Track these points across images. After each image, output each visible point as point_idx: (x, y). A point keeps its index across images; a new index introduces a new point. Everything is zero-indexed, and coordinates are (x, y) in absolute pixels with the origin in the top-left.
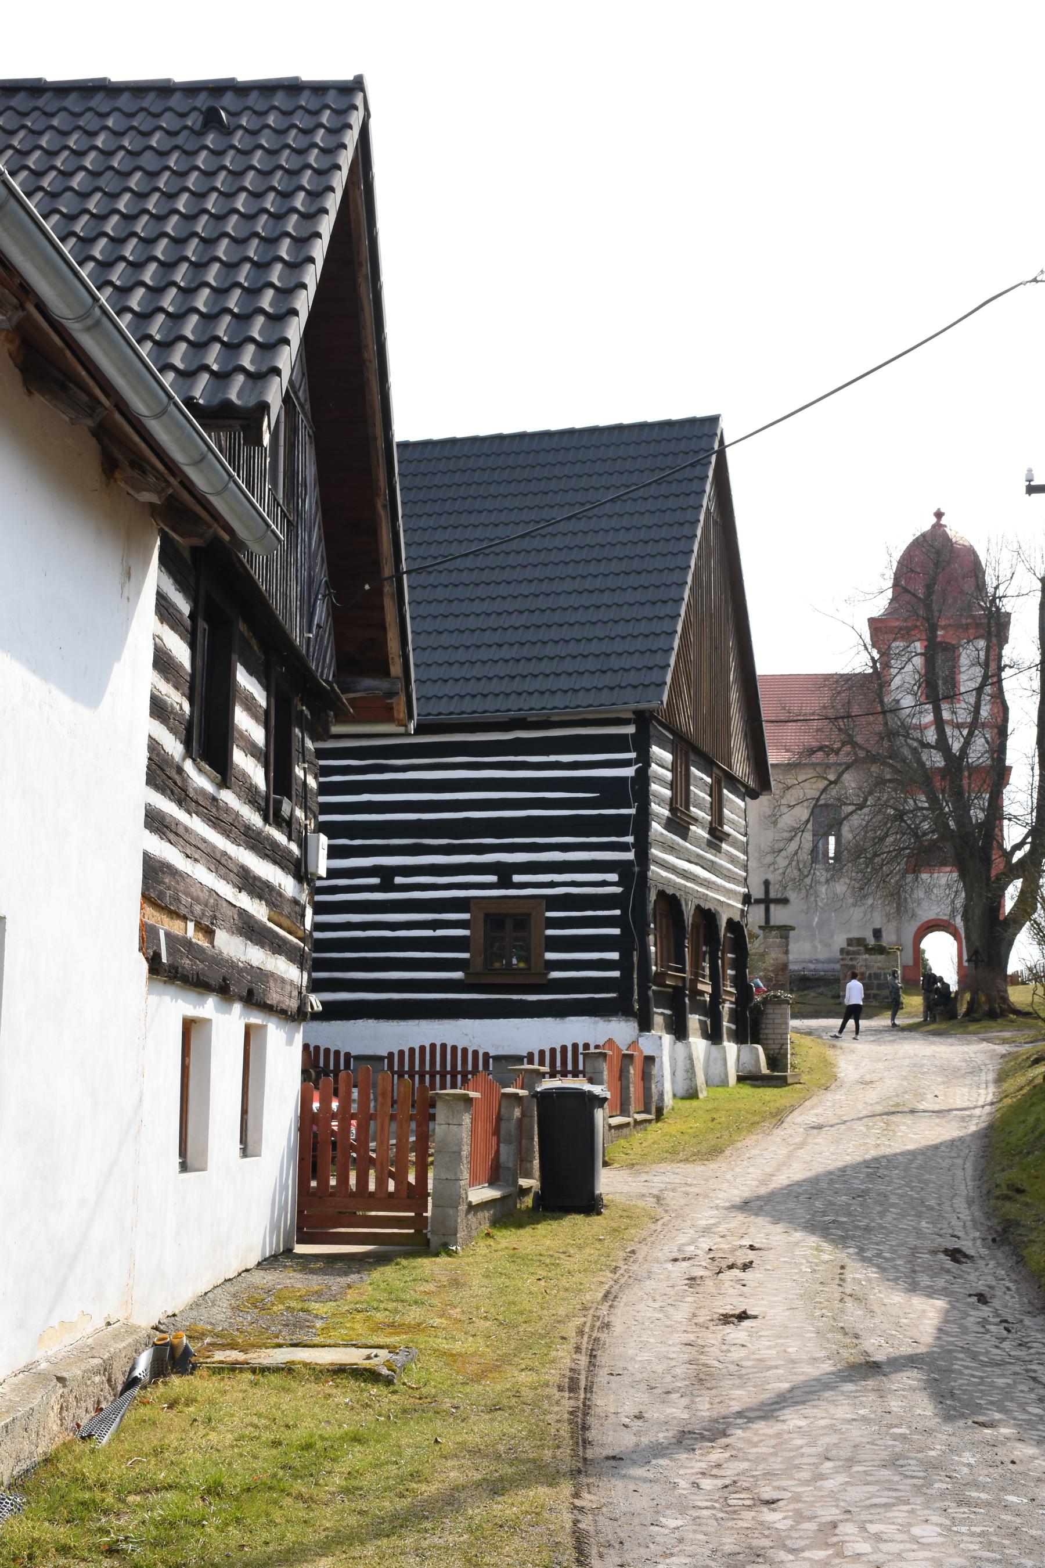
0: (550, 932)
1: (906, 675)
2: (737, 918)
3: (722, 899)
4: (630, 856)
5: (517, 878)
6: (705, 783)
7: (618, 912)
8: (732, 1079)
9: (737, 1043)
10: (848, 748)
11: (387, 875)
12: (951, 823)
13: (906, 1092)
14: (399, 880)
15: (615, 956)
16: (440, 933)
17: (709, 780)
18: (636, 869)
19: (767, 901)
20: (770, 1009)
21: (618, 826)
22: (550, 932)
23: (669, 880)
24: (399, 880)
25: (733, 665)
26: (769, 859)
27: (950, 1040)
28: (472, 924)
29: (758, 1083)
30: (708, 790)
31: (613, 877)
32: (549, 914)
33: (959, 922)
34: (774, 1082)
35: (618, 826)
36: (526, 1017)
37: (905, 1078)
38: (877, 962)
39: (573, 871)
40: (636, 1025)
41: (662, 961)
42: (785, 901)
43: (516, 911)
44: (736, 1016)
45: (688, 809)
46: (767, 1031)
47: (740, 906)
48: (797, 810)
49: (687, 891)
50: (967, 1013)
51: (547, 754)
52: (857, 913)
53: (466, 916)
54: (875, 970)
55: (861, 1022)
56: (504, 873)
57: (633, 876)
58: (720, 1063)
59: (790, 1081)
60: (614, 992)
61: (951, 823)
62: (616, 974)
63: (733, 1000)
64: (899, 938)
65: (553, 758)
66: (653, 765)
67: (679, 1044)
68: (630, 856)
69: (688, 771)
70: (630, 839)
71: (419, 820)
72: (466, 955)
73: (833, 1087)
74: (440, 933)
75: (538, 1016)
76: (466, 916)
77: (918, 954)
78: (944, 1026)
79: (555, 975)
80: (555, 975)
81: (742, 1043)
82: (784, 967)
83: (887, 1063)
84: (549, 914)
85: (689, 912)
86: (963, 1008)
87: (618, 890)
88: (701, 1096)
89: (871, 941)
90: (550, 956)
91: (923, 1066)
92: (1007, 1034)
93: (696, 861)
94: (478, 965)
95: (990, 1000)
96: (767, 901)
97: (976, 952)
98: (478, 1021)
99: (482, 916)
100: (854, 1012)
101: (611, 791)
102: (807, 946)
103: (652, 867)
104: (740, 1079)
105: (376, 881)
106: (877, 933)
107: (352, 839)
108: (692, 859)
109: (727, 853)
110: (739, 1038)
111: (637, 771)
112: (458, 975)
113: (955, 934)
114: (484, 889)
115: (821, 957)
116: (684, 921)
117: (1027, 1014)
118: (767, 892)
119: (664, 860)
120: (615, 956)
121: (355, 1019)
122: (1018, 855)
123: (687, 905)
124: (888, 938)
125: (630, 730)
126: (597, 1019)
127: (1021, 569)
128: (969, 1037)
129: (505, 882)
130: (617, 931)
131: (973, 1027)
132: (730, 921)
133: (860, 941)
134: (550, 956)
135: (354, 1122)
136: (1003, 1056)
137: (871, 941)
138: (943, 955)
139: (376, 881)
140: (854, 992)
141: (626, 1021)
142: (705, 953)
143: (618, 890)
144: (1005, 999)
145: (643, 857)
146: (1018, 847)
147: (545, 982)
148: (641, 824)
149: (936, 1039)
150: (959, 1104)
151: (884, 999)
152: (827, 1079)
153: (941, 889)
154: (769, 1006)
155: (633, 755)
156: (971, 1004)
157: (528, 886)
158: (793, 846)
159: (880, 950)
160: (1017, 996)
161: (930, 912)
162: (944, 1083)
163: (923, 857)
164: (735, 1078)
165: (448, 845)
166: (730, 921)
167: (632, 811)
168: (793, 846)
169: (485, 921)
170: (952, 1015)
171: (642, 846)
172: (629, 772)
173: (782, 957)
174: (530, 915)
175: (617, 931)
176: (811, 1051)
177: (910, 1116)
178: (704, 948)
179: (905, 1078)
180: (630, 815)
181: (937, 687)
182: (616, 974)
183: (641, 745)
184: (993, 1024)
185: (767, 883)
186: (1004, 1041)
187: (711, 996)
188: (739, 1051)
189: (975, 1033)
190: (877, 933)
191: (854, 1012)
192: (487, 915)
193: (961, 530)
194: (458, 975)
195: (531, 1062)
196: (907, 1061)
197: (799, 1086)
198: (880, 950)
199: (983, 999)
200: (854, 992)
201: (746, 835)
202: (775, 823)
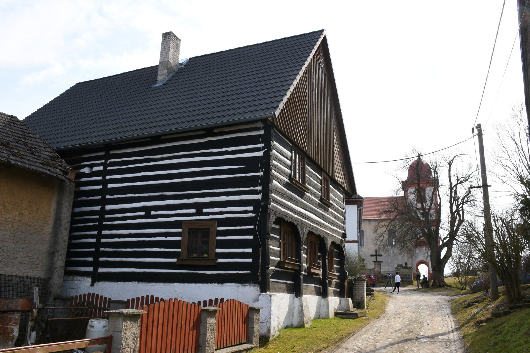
0: (219, 238)
1: (412, 197)
2: (338, 242)
3: (328, 232)
4: (259, 197)
5: (205, 210)
6: (318, 178)
7: (252, 227)
8: (332, 315)
9: (340, 297)
10: (396, 211)
11: (147, 210)
12: (426, 230)
13: (414, 322)
14: (153, 213)
15: (250, 250)
16: (169, 238)
17: (320, 177)
18: (262, 204)
19: (376, 255)
20: (357, 283)
21: (253, 181)
22: (219, 238)
23: (288, 214)
24: (153, 213)
25: (335, 137)
26: (375, 242)
27: (428, 294)
28: (182, 234)
29: (344, 316)
30: (320, 182)
31: (251, 208)
32: (219, 229)
33: (429, 261)
34: (352, 316)
35: (253, 181)
36: (119, 281)
37: (414, 312)
38: (406, 271)
39: (233, 205)
40: (259, 288)
41: (310, 261)
42: (381, 255)
43: (204, 227)
44: (340, 285)
45: (305, 184)
46: (356, 292)
47: (340, 238)
48: (382, 228)
49: (302, 223)
50: (433, 286)
51: (222, 148)
52: (400, 257)
53: (180, 230)
54: (405, 273)
55: (400, 288)
56: (199, 207)
57: (262, 208)
58: (326, 307)
59: (359, 315)
60: (249, 270)
61: (426, 230)
62: (250, 260)
63: (337, 278)
64: (412, 264)
65: (224, 149)
66: (274, 151)
67: (296, 299)
68: (259, 197)
69: (304, 169)
70: (260, 188)
71: (164, 183)
72: (179, 250)
73: (382, 317)
74: (169, 238)
75: (211, 283)
76: (180, 230)
77: (417, 270)
78: (426, 290)
79: (220, 260)
80: (220, 260)
81: (342, 297)
82: (380, 272)
83: (407, 304)
84: (219, 229)
85: (304, 233)
86: (431, 284)
87: (253, 215)
88: (306, 326)
89: (404, 265)
90: (218, 250)
91: (420, 306)
92: (446, 292)
93: (310, 210)
94: (184, 256)
95: (439, 282)
96: (376, 255)
97: (435, 268)
98: (182, 284)
99: (187, 230)
100: (397, 285)
101: (251, 164)
102: (387, 267)
103: (272, 203)
104: (336, 314)
105: (143, 213)
106: (406, 264)
107: (135, 194)
108: (307, 209)
109: (332, 213)
110: (340, 294)
111: (264, 153)
112: (174, 260)
113: (428, 265)
114: (189, 216)
115: (391, 270)
116: (300, 237)
117: (450, 286)
118: (376, 253)
119: (283, 202)
120: (250, 250)
121: (129, 281)
122: (445, 241)
123: (302, 229)
124: (409, 265)
125: (262, 132)
126: (239, 285)
127: (442, 161)
128: (434, 293)
129: (199, 213)
130: (251, 237)
131: (435, 290)
132: (333, 243)
133: (401, 266)
134: (218, 250)
135: (212, 321)
136: (449, 301)
137: (404, 265)
138: (424, 270)
139: (143, 213)
140: (398, 279)
141: (254, 286)
142: (319, 256)
143: (253, 215)
144: (444, 282)
145: (266, 198)
146: (445, 238)
147: (213, 264)
148: (266, 181)
149: (424, 294)
150: (441, 330)
151: (406, 281)
152: (382, 310)
153: (423, 253)
154: (357, 282)
155: (263, 145)
156: (433, 283)
157: (211, 214)
158: (381, 238)
159: (407, 268)
160: (447, 281)
161: (421, 257)
162: (430, 315)
163: (419, 244)
164: (334, 314)
165: (175, 195)
166: (333, 243)
167: (262, 173)
168: (381, 238)
169: (189, 232)
170: (428, 286)
171: (266, 192)
172: (260, 154)
173: (379, 270)
174: (209, 229)
175: (251, 237)
176: (380, 299)
177: (416, 344)
178: (319, 254)
179: (414, 312)
180: (259, 176)
181: (421, 198)
182: (250, 260)
183: (267, 140)
184: (441, 289)
185: (381, 255)
186: (446, 295)
187: (322, 275)
188: (340, 300)
189: (436, 292)
190: (406, 264)
191: (397, 285)
192: (190, 230)
193: (426, 159)
194: (174, 260)
195: (211, 305)
196: (414, 304)
197: (364, 318)
198: (407, 268)
199: (437, 281)
200: (398, 279)
201: (343, 209)
202: (376, 232)
